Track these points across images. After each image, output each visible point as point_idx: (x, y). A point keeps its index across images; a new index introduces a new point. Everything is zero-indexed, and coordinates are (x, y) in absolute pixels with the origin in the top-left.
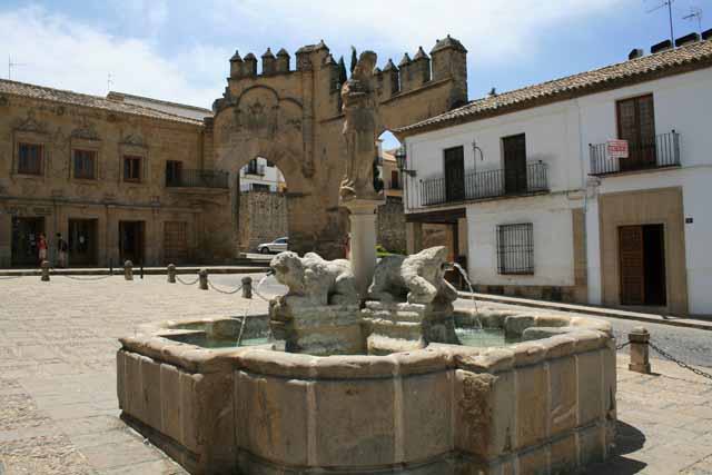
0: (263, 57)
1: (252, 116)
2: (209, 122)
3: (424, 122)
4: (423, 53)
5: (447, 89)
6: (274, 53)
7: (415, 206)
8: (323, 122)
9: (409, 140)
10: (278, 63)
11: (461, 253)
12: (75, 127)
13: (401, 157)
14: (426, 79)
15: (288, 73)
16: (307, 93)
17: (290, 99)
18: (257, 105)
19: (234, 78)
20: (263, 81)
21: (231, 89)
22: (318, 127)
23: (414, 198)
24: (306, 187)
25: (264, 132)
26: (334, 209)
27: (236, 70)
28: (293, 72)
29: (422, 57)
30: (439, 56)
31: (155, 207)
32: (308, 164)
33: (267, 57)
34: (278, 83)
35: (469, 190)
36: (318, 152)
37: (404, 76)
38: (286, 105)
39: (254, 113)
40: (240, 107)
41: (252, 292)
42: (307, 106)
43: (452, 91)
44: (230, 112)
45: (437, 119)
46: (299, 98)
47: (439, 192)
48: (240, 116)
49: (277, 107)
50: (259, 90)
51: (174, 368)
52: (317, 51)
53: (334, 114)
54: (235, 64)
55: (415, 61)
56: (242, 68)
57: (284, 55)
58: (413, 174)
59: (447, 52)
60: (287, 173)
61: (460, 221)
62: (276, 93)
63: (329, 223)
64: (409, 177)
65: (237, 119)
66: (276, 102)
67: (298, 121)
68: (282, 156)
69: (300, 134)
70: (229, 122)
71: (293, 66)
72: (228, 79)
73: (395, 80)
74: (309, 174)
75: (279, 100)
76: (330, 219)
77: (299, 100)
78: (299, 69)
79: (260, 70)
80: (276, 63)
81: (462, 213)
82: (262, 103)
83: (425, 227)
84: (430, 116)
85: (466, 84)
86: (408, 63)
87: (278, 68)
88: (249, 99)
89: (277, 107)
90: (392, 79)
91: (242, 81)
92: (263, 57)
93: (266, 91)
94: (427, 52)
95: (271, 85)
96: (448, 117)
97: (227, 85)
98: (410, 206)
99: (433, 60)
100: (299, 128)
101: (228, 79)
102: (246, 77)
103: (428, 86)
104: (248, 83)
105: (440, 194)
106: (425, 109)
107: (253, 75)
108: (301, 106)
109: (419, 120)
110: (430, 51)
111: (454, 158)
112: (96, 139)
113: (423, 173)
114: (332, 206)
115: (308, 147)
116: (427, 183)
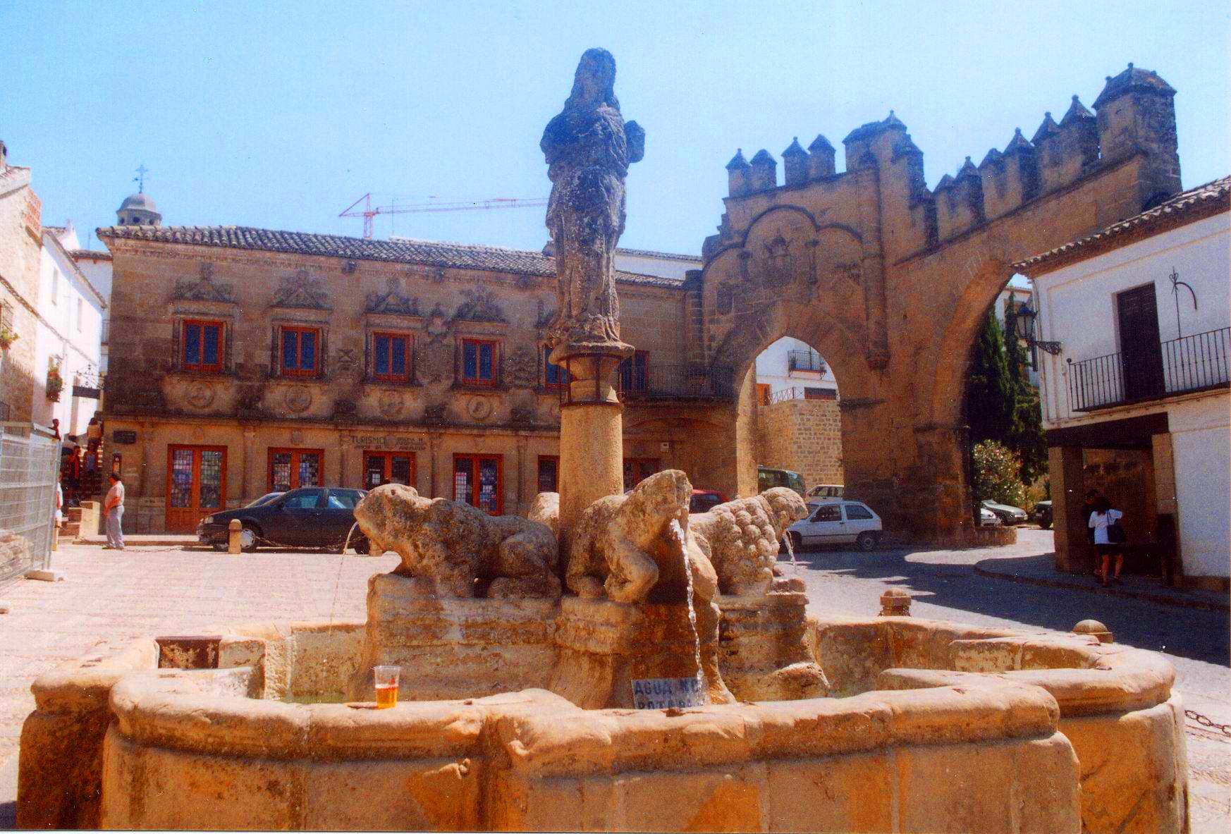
0: (845, 142)
2: (695, 279)
5: (1131, 170)
6: (805, 144)
7: (1064, 415)
8: (904, 261)
12: (463, 300)
15: (830, 178)
17: (835, 226)
18: (780, 241)
19: (737, 197)
21: (732, 217)
24: (875, 387)
25: (793, 289)
26: (930, 427)
27: (741, 181)
28: (841, 175)
30: (1111, 108)
33: (793, 152)
34: (814, 198)
35: (1173, 377)
36: (893, 320)
40: (749, 248)
42: (867, 235)
43: (1143, 175)
47: (1110, 385)
53: (920, 243)
54: (737, 172)
55: (1064, 125)
57: (822, 145)
58: (1055, 348)
59: (1128, 97)
61: (1156, 439)
62: (811, 217)
63: (920, 456)
64: (1048, 356)
65: (745, 273)
67: (855, 266)
70: (142, 305)
71: (841, 166)
72: (725, 200)
74: (880, 364)
75: (818, 229)
76: (920, 447)
77: (854, 226)
78: (850, 171)
79: (781, 180)
80: (810, 165)
81: (1160, 424)
83: (1095, 457)
85: (1176, 158)
86: (1048, 131)
88: (764, 232)
89: (815, 243)
91: (751, 202)
92: (845, 142)
94: (1088, 101)
98: (1053, 415)
100: (856, 278)
101: (725, 200)
103: (1093, 169)
104: (761, 204)
108: (858, 236)
111: (1137, 312)
112: (318, 307)
113: (1074, 349)
114: (922, 421)
115: (875, 312)
116: (1081, 367)
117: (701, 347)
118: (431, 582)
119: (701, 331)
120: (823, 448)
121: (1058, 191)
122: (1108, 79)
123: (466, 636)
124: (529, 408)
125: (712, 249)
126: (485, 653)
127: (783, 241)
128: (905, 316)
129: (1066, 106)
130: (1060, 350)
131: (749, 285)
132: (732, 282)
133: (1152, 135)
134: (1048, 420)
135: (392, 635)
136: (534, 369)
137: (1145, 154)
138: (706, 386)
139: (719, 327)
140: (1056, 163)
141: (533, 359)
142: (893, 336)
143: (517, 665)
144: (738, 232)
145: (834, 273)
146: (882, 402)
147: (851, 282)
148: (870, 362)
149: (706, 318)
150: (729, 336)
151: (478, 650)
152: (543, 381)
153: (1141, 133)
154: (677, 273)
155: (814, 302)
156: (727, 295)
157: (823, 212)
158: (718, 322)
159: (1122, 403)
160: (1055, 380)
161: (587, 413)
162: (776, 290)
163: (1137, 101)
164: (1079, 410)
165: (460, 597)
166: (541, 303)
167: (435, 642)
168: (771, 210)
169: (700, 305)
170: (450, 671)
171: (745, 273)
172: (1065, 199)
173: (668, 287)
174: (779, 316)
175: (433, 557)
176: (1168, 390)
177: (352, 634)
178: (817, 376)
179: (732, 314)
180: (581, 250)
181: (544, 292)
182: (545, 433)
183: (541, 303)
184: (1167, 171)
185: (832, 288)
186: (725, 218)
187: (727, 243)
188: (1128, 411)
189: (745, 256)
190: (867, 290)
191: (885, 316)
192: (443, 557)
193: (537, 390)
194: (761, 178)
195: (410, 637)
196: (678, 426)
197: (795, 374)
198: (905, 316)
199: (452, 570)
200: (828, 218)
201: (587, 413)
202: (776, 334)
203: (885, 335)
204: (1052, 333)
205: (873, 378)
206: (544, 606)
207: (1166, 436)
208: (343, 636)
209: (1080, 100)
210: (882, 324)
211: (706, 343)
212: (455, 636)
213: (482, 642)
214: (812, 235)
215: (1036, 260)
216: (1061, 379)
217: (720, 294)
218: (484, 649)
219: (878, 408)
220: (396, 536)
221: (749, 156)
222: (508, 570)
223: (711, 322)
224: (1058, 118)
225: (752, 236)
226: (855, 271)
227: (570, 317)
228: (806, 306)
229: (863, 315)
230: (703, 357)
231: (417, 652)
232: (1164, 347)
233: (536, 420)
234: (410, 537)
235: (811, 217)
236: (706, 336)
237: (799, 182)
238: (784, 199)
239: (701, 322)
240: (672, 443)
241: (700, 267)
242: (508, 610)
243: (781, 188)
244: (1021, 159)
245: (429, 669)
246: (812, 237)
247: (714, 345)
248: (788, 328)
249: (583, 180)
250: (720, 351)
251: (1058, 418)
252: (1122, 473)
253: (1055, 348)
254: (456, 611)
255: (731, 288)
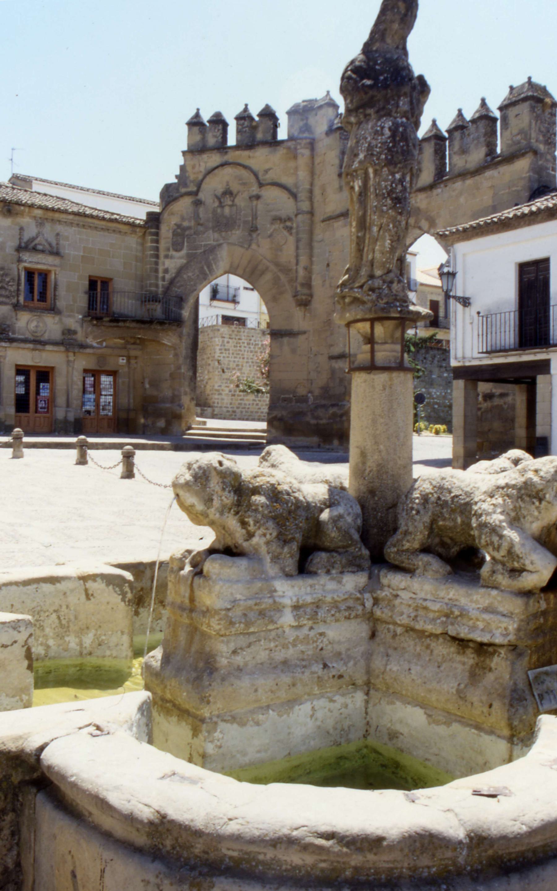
0: (289, 113)
1: (219, 210)
2: (154, 219)
3: (488, 219)
4: (438, 130)
5: (522, 165)
6: (255, 112)
7: (468, 354)
9: (462, 248)
10: (260, 129)
11: (540, 431)
13: (448, 273)
14: (491, 147)
15: (273, 142)
16: (303, 174)
18: (228, 192)
19: (194, 151)
20: (243, 156)
21: (189, 168)
22: (319, 228)
23: (467, 344)
24: (299, 320)
25: (237, 234)
27: (198, 138)
28: (282, 142)
29: (485, 118)
30: (512, 112)
31: (68, 342)
32: (302, 285)
33: (244, 118)
34: (259, 158)
37: (456, 147)
38: (271, 194)
39: (221, 206)
41: (135, 471)
42: (303, 195)
44: (183, 205)
45: (509, 213)
46: (288, 181)
48: (201, 210)
49: (258, 197)
50: (228, 170)
51: (346, 157)
52: (321, 107)
54: (196, 129)
55: (473, 121)
56: (205, 133)
57: (268, 114)
58: (466, 302)
59: (527, 104)
60: (271, 299)
61: (540, 379)
62: (256, 175)
64: (460, 307)
65: (196, 216)
66: (255, 189)
67: (290, 219)
68: (263, 273)
69: (291, 240)
72: (184, 153)
73: (440, 153)
74: (305, 303)
75: (261, 185)
78: (291, 138)
79: (232, 140)
80: (258, 128)
81: (544, 367)
82: (235, 192)
83: (484, 387)
84: (495, 209)
87: (259, 136)
88: (214, 185)
89: (258, 197)
90: (436, 152)
91: (205, 156)
92: (289, 113)
93: (245, 173)
95: (247, 163)
96: (526, 210)
97: (182, 163)
98: (460, 355)
99: (504, 119)
100: (289, 229)
101: (184, 153)
102: (212, 149)
103: (492, 161)
104: (214, 159)
105: (509, 336)
106: (487, 199)
107: (222, 147)
108: (294, 196)
109: (475, 216)
110: (498, 103)
114: (336, 350)
115: (304, 260)
116: (487, 317)
117: (157, 278)
118: (260, 560)
119: (157, 263)
120: (237, 365)
121: (464, 175)
122: (511, 88)
123: (297, 617)
124: (8, 323)
125: (169, 194)
126: (312, 633)
127: (231, 193)
128: (328, 265)
129: (477, 105)
130: (469, 304)
131: (201, 228)
132: (186, 224)
133: (541, 138)
134: (456, 358)
135: (232, 623)
136: (15, 288)
137: (536, 152)
138: (158, 310)
139: (172, 262)
140: (464, 151)
141: (13, 279)
142: (316, 282)
143: (339, 642)
144: (193, 182)
145: (272, 224)
146: (304, 333)
147: (285, 233)
148: (297, 301)
149: (162, 253)
150: (180, 271)
151: (305, 631)
152: (21, 299)
153: (533, 135)
154: (139, 214)
155: (254, 246)
156: (180, 235)
157: (266, 171)
158: (172, 257)
159: (514, 350)
160: (464, 327)
161: (391, 379)
162: (223, 234)
163: (533, 109)
164: (482, 353)
165: (288, 576)
166: (22, 229)
167: (271, 627)
168: (222, 165)
169: (157, 241)
170: (280, 655)
171: (196, 216)
172: (469, 182)
173: (132, 225)
174: (224, 256)
175: (264, 535)
176: (551, 342)
177: (58, 585)
178: (231, 305)
179: (184, 252)
180: (393, 207)
181: (25, 220)
182: (22, 345)
183: (22, 229)
184: (547, 169)
185: (270, 236)
186: (182, 168)
187: (183, 190)
188: (520, 355)
189: (198, 203)
190: (298, 241)
191: (311, 262)
192: (275, 534)
193: (16, 307)
194: (215, 136)
195: (248, 624)
196: (134, 343)
197: (215, 303)
198: (328, 265)
199: (283, 548)
200: (270, 176)
201: (391, 379)
202: (221, 271)
203: (310, 278)
204: (464, 292)
205: (298, 313)
206: (361, 579)
207: (548, 376)
208: (47, 587)
209: (464, 112)
210: (308, 270)
211: (161, 275)
212: (287, 619)
213: (310, 622)
214: (255, 189)
215: (458, 230)
216: (468, 327)
217: (175, 234)
218: (311, 628)
219: (302, 338)
220: (222, 513)
221: (206, 117)
222: (327, 544)
223: (167, 257)
224: (468, 115)
225: (204, 186)
226: (288, 224)
227: (372, 277)
228: (247, 249)
229: (293, 261)
230: (157, 286)
231: (252, 639)
232: (551, 308)
233: (14, 333)
234: (237, 513)
235: (256, 175)
236: (161, 268)
237: (248, 143)
238: (230, 156)
239: (157, 256)
240: (129, 358)
241: (157, 210)
242: (331, 585)
243: (231, 148)
244: (436, 144)
245: (263, 656)
246: (255, 193)
247: (168, 277)
248: (231, 266)
249: (394, 131)
250: (172, 282)
251: (464, 358)
252: (497, 401)
253: (466, 302)
254: (289, 591)
255: (185, 229)
